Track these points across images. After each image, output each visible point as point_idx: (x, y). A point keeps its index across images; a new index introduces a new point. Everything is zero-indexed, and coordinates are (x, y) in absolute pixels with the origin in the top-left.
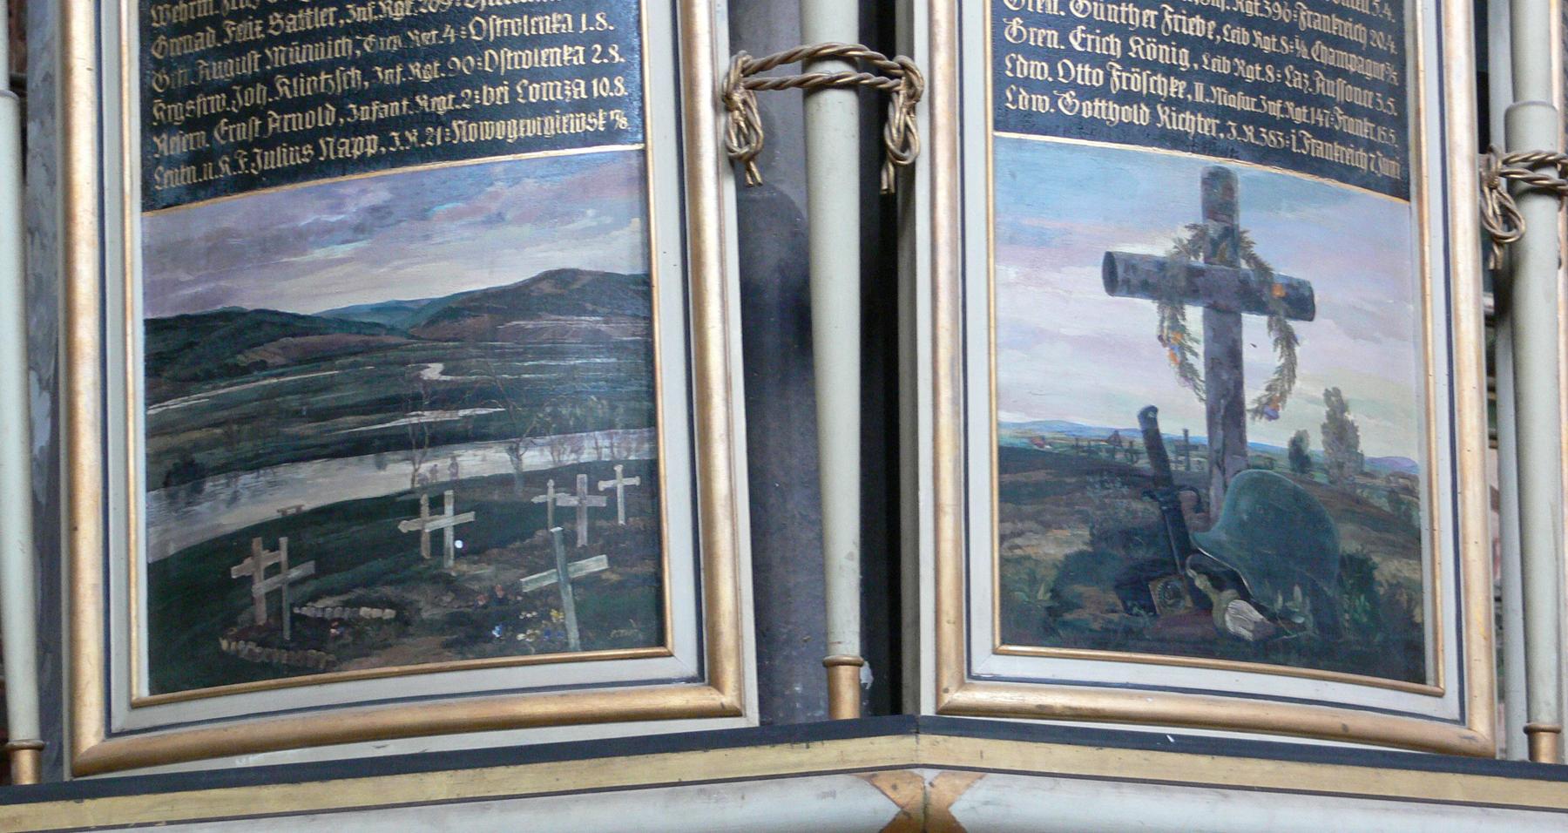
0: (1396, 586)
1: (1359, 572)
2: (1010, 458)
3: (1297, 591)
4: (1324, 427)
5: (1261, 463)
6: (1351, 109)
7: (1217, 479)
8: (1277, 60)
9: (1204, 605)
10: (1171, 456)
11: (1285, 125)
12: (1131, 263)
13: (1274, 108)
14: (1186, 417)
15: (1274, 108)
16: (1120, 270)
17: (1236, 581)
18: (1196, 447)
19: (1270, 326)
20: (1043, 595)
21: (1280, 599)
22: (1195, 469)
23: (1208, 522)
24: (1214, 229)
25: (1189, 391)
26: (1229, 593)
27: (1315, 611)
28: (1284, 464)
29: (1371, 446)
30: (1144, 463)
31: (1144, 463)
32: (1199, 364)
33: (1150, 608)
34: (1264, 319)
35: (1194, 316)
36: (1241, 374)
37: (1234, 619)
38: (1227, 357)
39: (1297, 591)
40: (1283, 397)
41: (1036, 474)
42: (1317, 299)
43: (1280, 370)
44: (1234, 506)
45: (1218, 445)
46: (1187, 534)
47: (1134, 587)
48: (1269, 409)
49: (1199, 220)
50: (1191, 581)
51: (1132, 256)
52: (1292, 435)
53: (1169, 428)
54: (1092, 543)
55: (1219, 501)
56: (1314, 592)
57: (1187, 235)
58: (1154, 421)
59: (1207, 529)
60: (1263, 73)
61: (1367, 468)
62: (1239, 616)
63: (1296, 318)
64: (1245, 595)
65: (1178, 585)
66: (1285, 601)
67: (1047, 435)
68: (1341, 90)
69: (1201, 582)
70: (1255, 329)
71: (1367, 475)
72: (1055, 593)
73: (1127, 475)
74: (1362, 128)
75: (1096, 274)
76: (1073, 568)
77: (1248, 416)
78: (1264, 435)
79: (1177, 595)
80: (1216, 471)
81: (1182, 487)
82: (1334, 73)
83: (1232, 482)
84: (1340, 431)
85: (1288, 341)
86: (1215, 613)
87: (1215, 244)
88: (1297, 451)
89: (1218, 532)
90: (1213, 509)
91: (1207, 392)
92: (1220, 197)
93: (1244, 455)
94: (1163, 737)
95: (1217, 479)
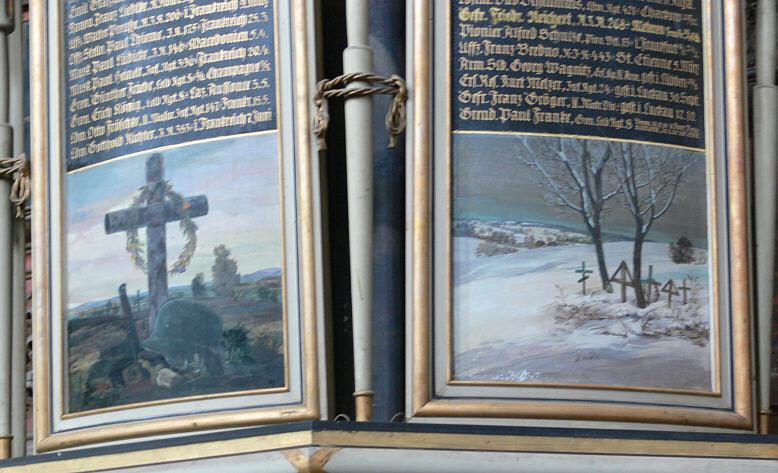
0: (264, 338)
1: (239, 337)
2: (71, 326)
3: (196, 356)
4: (214, 268)
5: (175, 296)
6: (233, 96)
7: (153, 311)
8: (186, 88)
9: (146, 374)
10: (132, 305)
11: (191, 119)
12: (115, 215)
13: (184, 113)
14: (139, 284)
15: (184, 113)
16: (111, 220)
17: (162, 358)
18: (142, 298)
19: (181, 225)
20: (84, 387)
21: (186, 363)
22: (142, 309)
23: (148, 334)
24: (151, 186)
25: (140, 271)
26: (158, 366)
27: (207, 365)
28: (190, 293)
29: (246, 268)
30: (120, 313)
31: (120, 313)
32: (144, 256)
33: (123, 382)
34: (178, 222)
35: (142, 233)
36: (165, 255)
37: (161, 379)
38: (159, 247)
39: (196, 356)
40: (189, 259)
41: (79, 330)
42: (209, 203)
43: (187, 246)
44: (161, 322)
45: (153, 293)
46: (138, 342)
47: (116, 374)
48: (180, 268)
49: (145, 184)
50: (140, 365)
51: (115, 213)
52: (194, 277)
53: (131, 292)
54: (101, 357)
55: (154, 323)
56: (206, 354)
57: (138, 193)
58: (124, 290)
59: (147, 337)
60: (625, 124)
61: (242, 281)
62: (164, 376)
63: (197, 215)
64: (167, 366)
65: (136, 368)
66: (189, 362)
67: (85, 310)
68: (228, 87)
69: (145, 364)
70: (174, 234)
71: (241, 285)
72: (88, 385)
73: (112, 320)
74: (243, 102)
75: (102, 226)
76: (96, 370)
77: (169, 275)
78: (178, 282)
79: (134, 373)
80: (152, 307)
81: (136, 319)
82: (220, 81)
83: (160, 310)
84: (224, 264)
85: (191, 229)
86: (152, 378)
87: (152, 193)
88: (197, 285)
89: (153, 338)
90: (151, 326)
91: (149, 268)
92: (155, 168)
93: (167, 295)
94: (56, 454)
95: (153, 311)
